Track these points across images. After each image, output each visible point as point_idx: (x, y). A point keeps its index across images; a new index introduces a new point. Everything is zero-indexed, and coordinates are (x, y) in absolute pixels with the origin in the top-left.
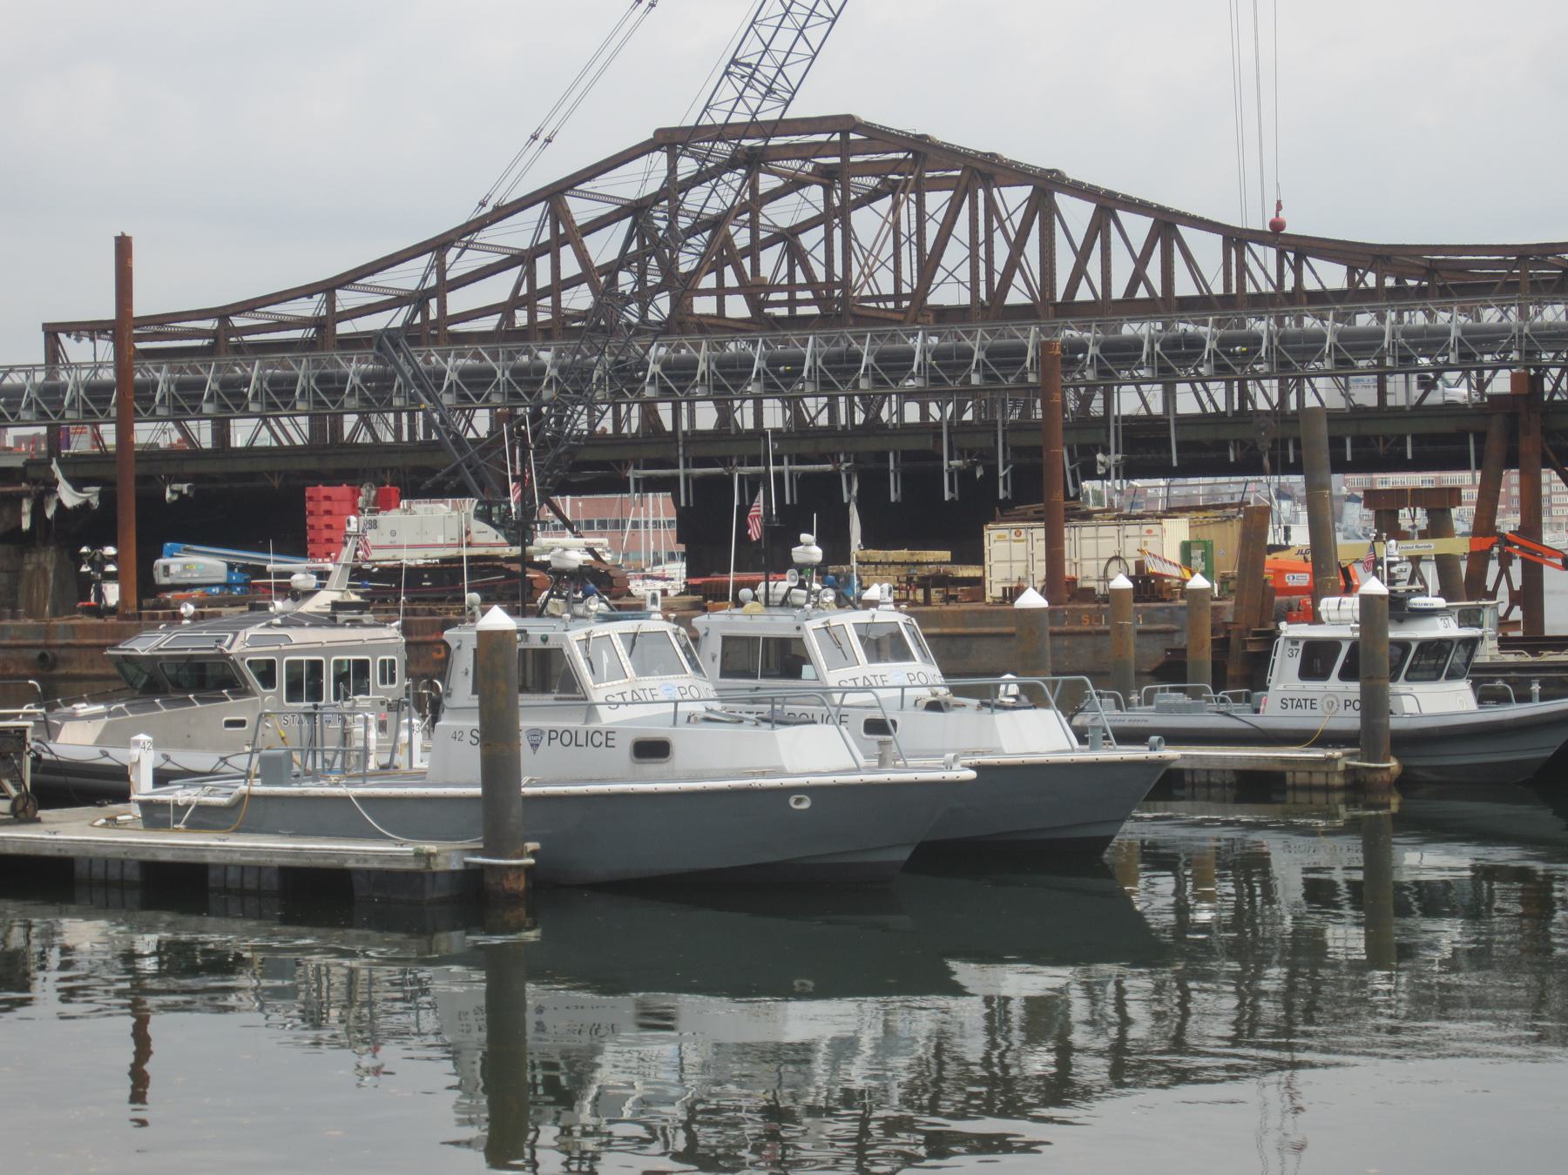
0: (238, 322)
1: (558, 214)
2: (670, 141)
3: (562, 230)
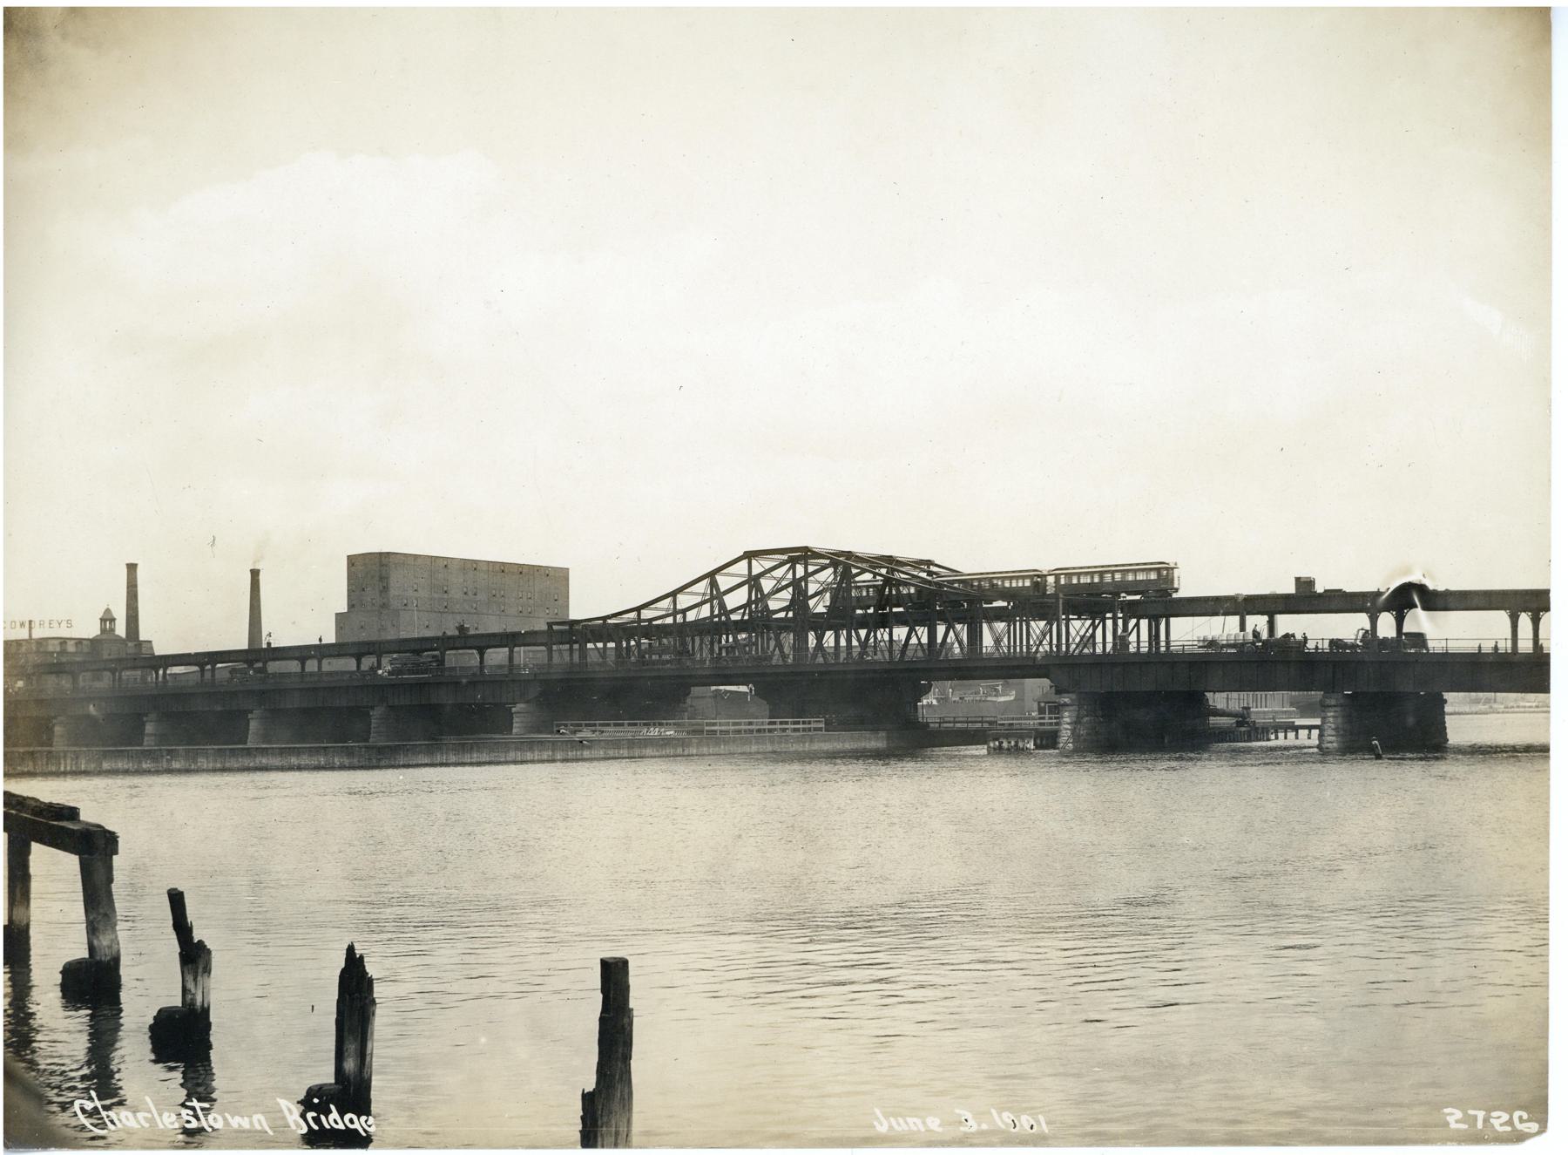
0: (646, 614)
1: (714, 584)
2: (750, 556)
3: (715, 592)
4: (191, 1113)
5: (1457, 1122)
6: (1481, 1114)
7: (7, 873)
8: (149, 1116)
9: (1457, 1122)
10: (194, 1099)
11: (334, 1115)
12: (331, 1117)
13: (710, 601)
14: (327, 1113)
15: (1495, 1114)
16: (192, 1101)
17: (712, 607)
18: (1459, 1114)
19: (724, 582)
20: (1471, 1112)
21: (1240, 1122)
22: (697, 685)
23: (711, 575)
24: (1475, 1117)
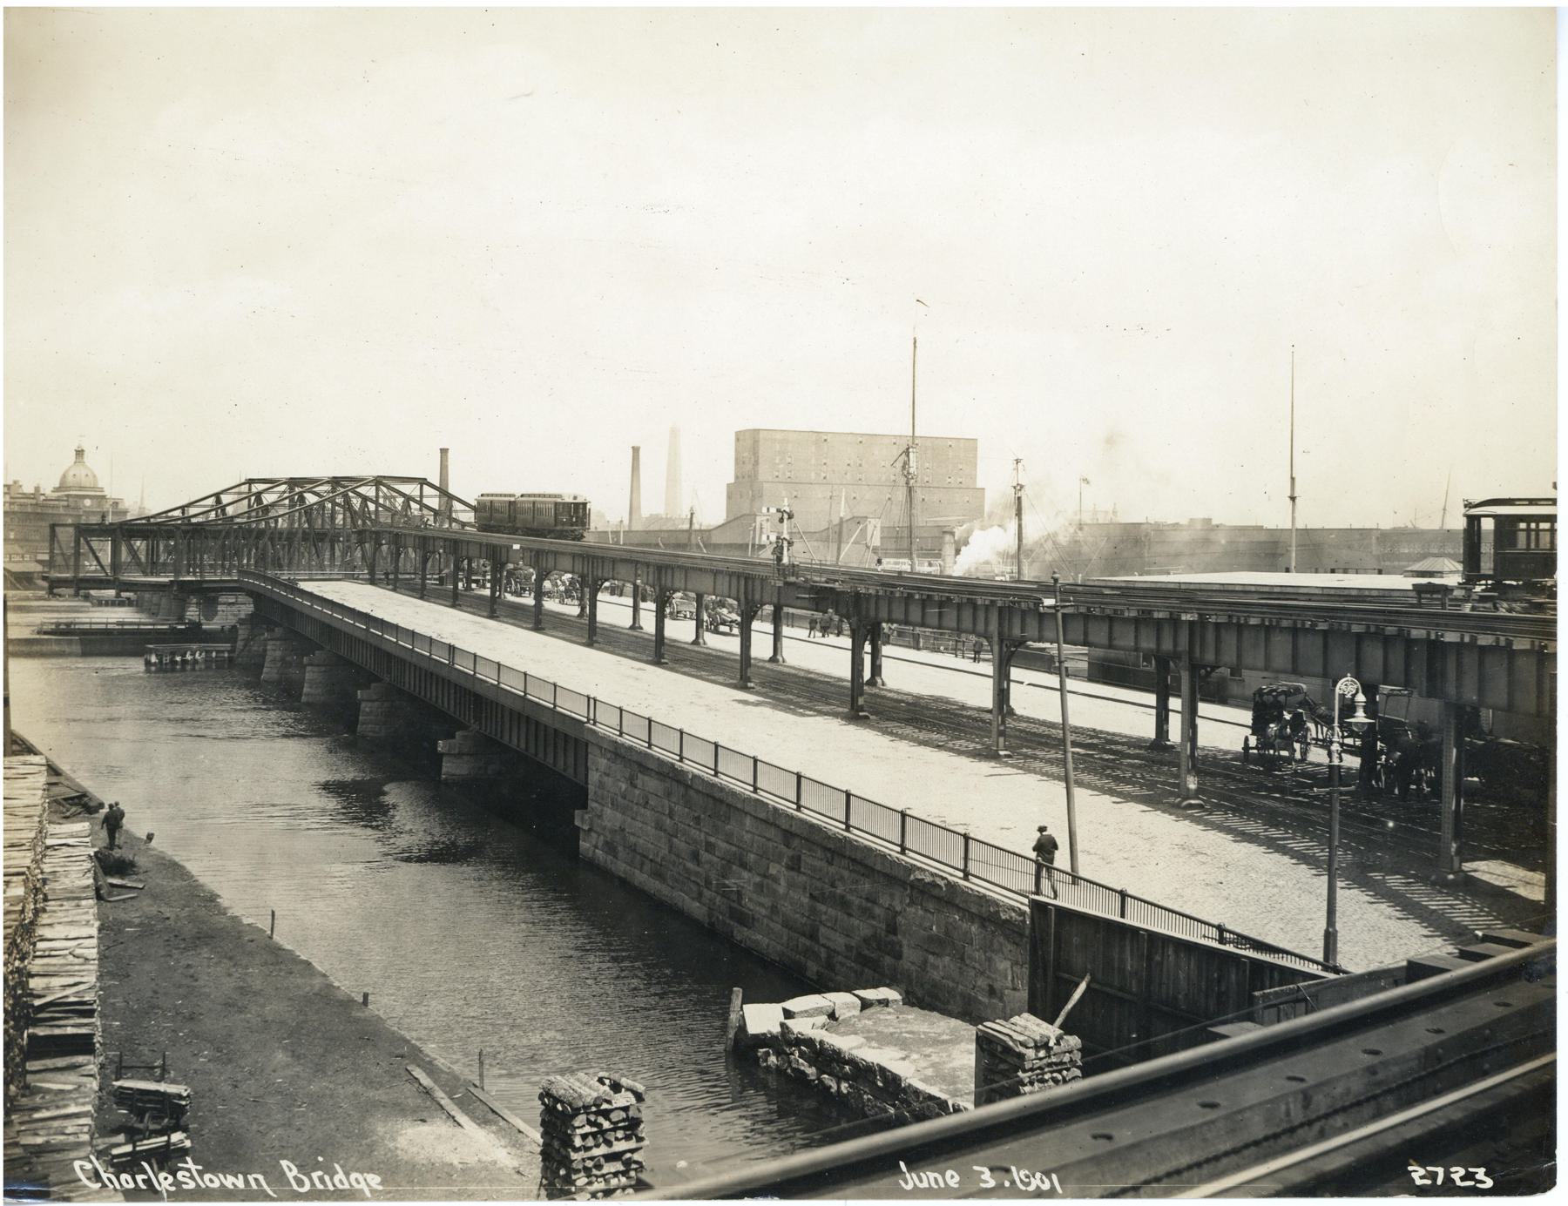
1: (218, 501)
2: (250, 482)
4: (188, 1174)
5: (1421, 1178)
6: (1440, 1171)
7: (1063, 1102)
8: (146, 1177)
9: (1421, 1178)
10: (188, 1159)
11: (340, 1175)
12: (336, 1179)
13: (216, 510)
14: (332, 1174)
15: (1453, 1169)
16: (187, 1163)
17: (216, 514)
18: (1422, 1172)
19: (226, 499)
20: (1471, 1170)
21: (740, 701)
22: (148, 546)
23: (217, 495)
24: (1436, 1174)
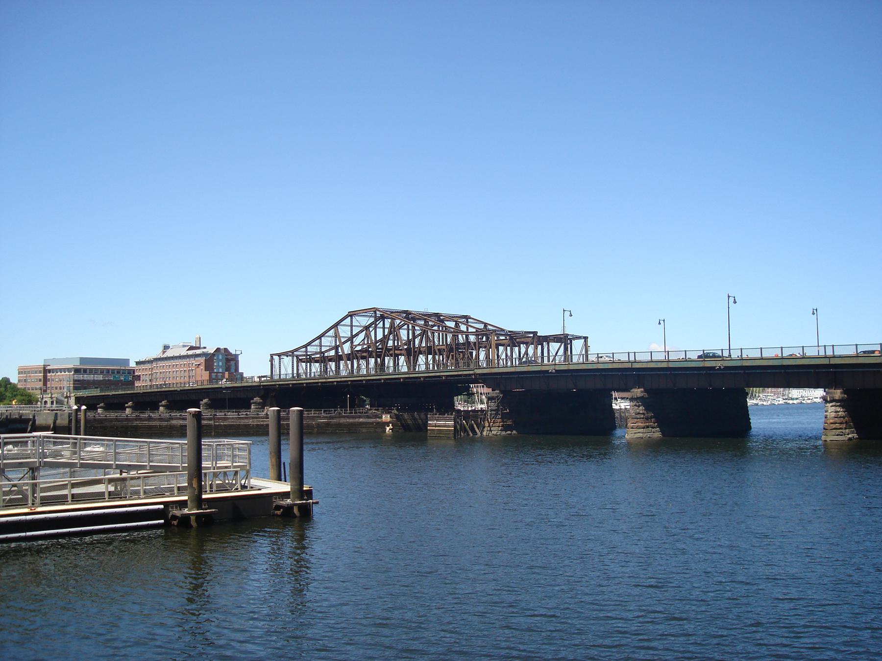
2: (351, 315)
